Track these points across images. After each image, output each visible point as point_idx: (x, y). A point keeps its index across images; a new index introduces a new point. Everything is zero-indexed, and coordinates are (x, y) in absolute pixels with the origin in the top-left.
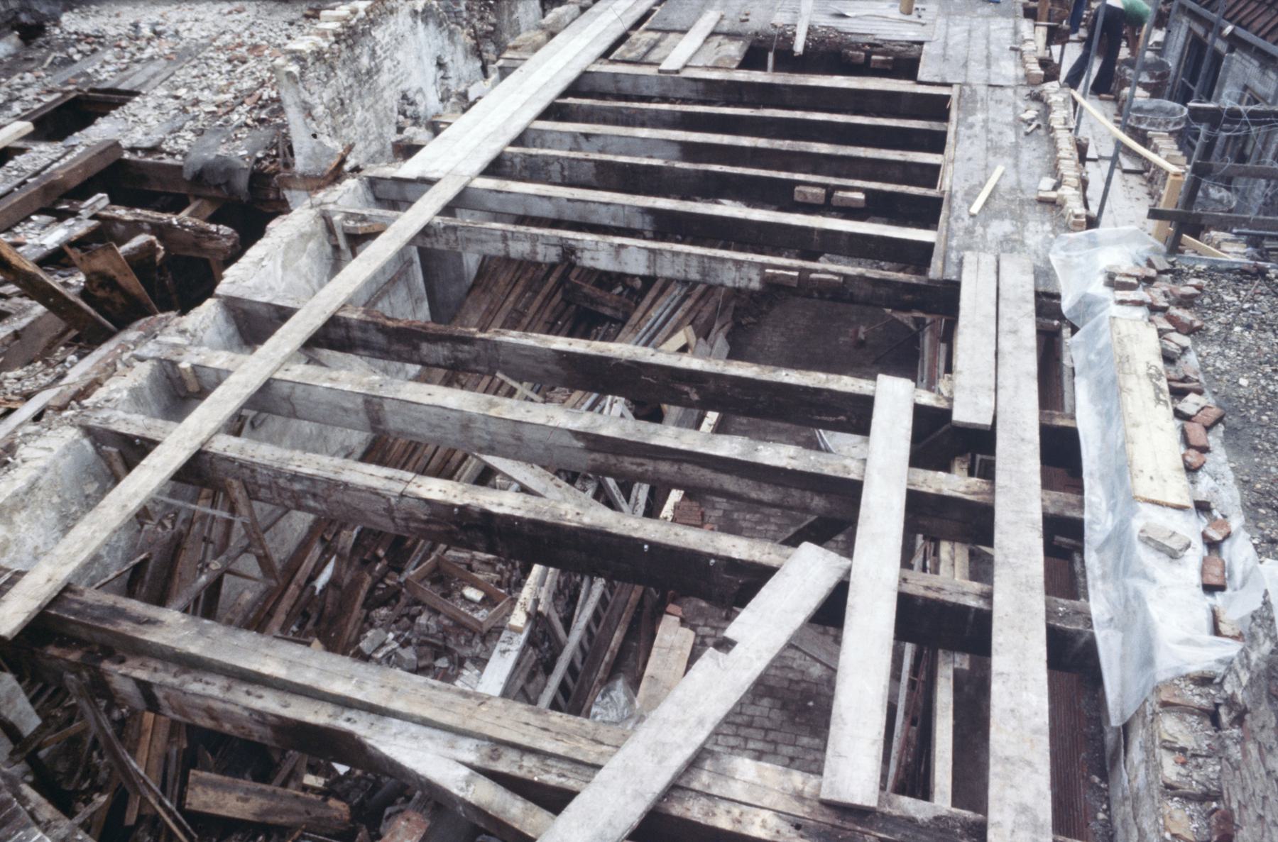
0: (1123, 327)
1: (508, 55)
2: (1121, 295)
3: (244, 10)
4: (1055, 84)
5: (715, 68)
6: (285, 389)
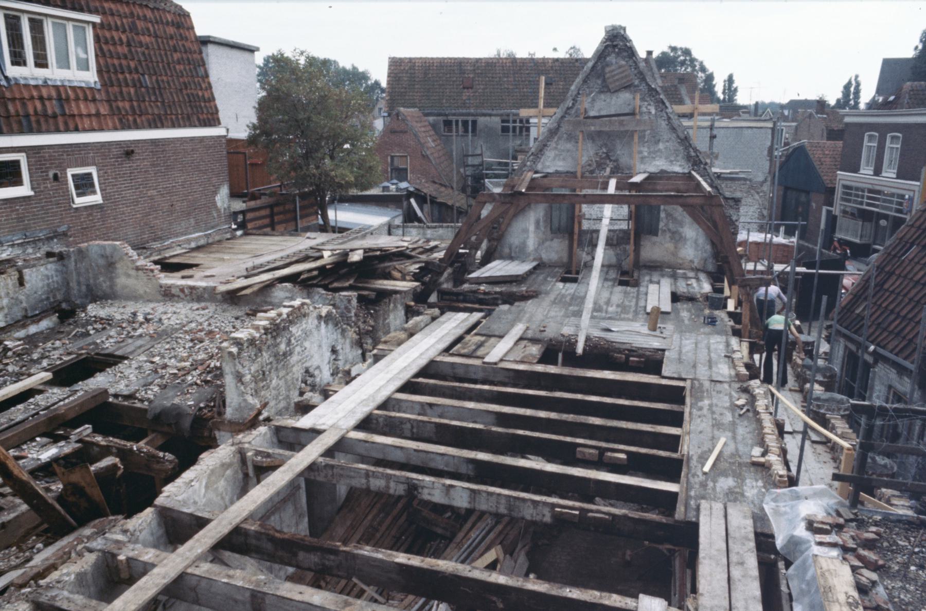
0: (824, 564)
1: (380, 347)
2: (819, 538)
3: (207, 308)
4: (757, 382)
5: (522, 362)
6: (194, 581)
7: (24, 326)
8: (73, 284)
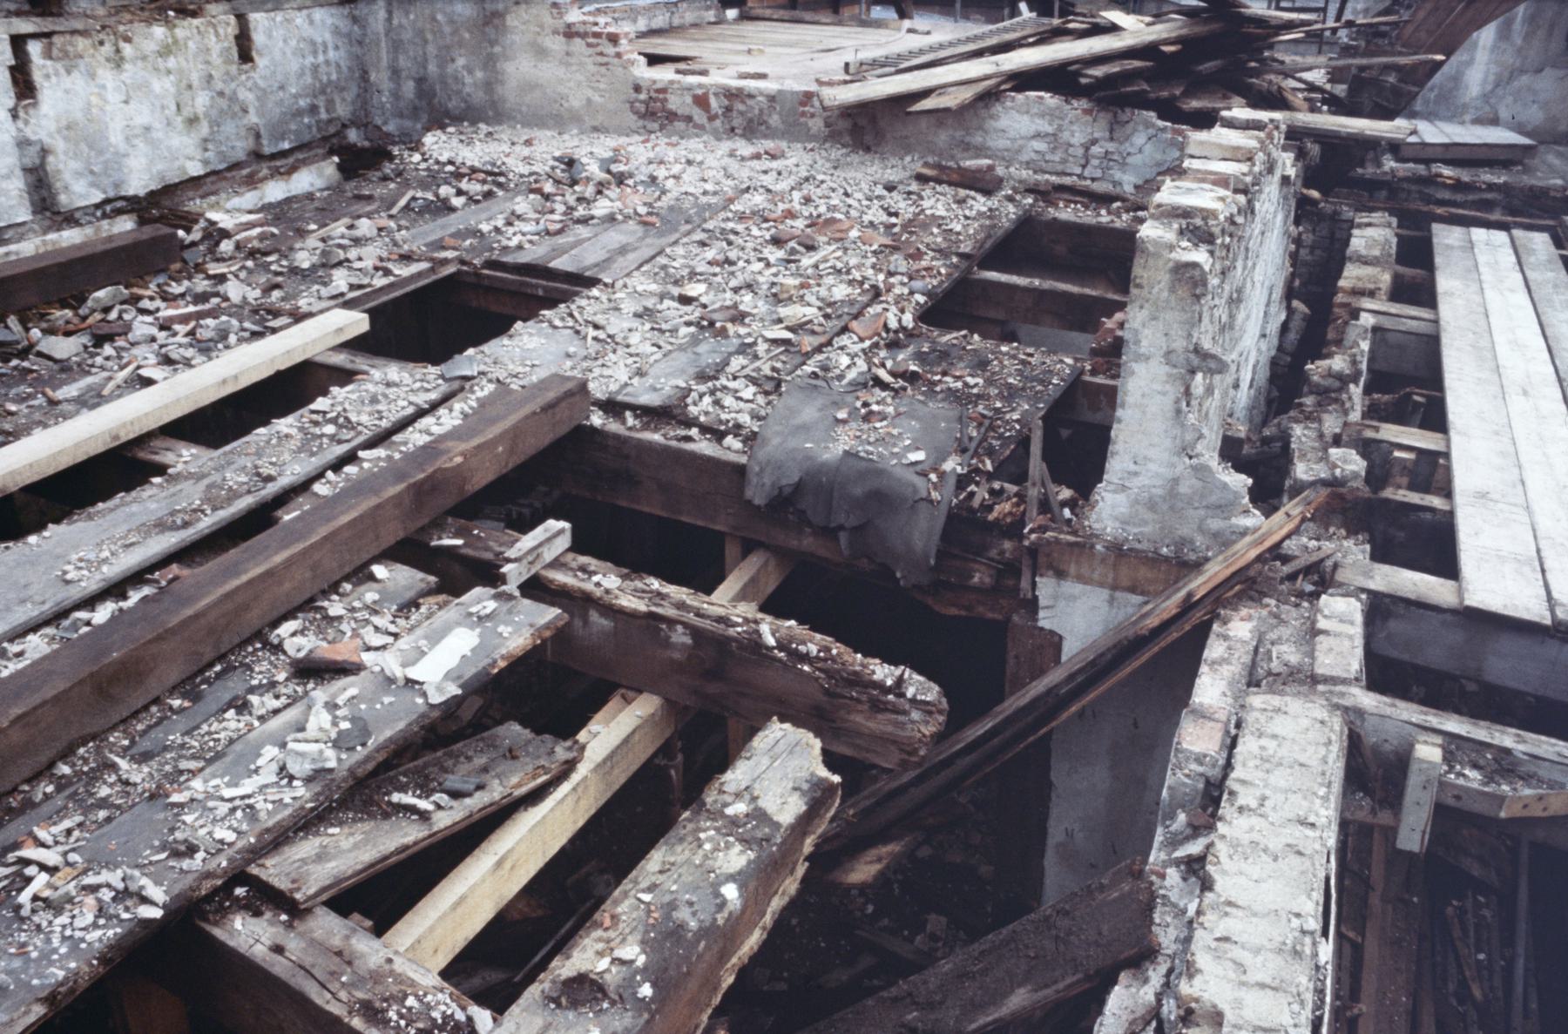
7: (252, 182)
8: (380, 77)
